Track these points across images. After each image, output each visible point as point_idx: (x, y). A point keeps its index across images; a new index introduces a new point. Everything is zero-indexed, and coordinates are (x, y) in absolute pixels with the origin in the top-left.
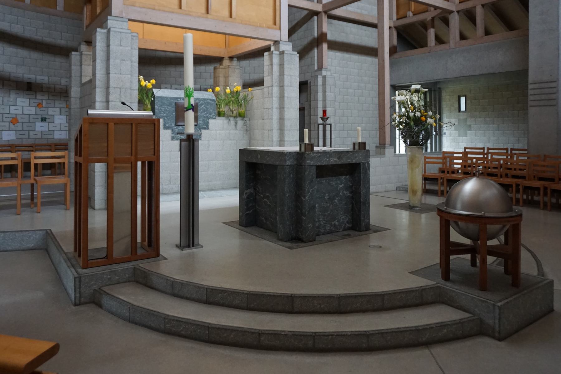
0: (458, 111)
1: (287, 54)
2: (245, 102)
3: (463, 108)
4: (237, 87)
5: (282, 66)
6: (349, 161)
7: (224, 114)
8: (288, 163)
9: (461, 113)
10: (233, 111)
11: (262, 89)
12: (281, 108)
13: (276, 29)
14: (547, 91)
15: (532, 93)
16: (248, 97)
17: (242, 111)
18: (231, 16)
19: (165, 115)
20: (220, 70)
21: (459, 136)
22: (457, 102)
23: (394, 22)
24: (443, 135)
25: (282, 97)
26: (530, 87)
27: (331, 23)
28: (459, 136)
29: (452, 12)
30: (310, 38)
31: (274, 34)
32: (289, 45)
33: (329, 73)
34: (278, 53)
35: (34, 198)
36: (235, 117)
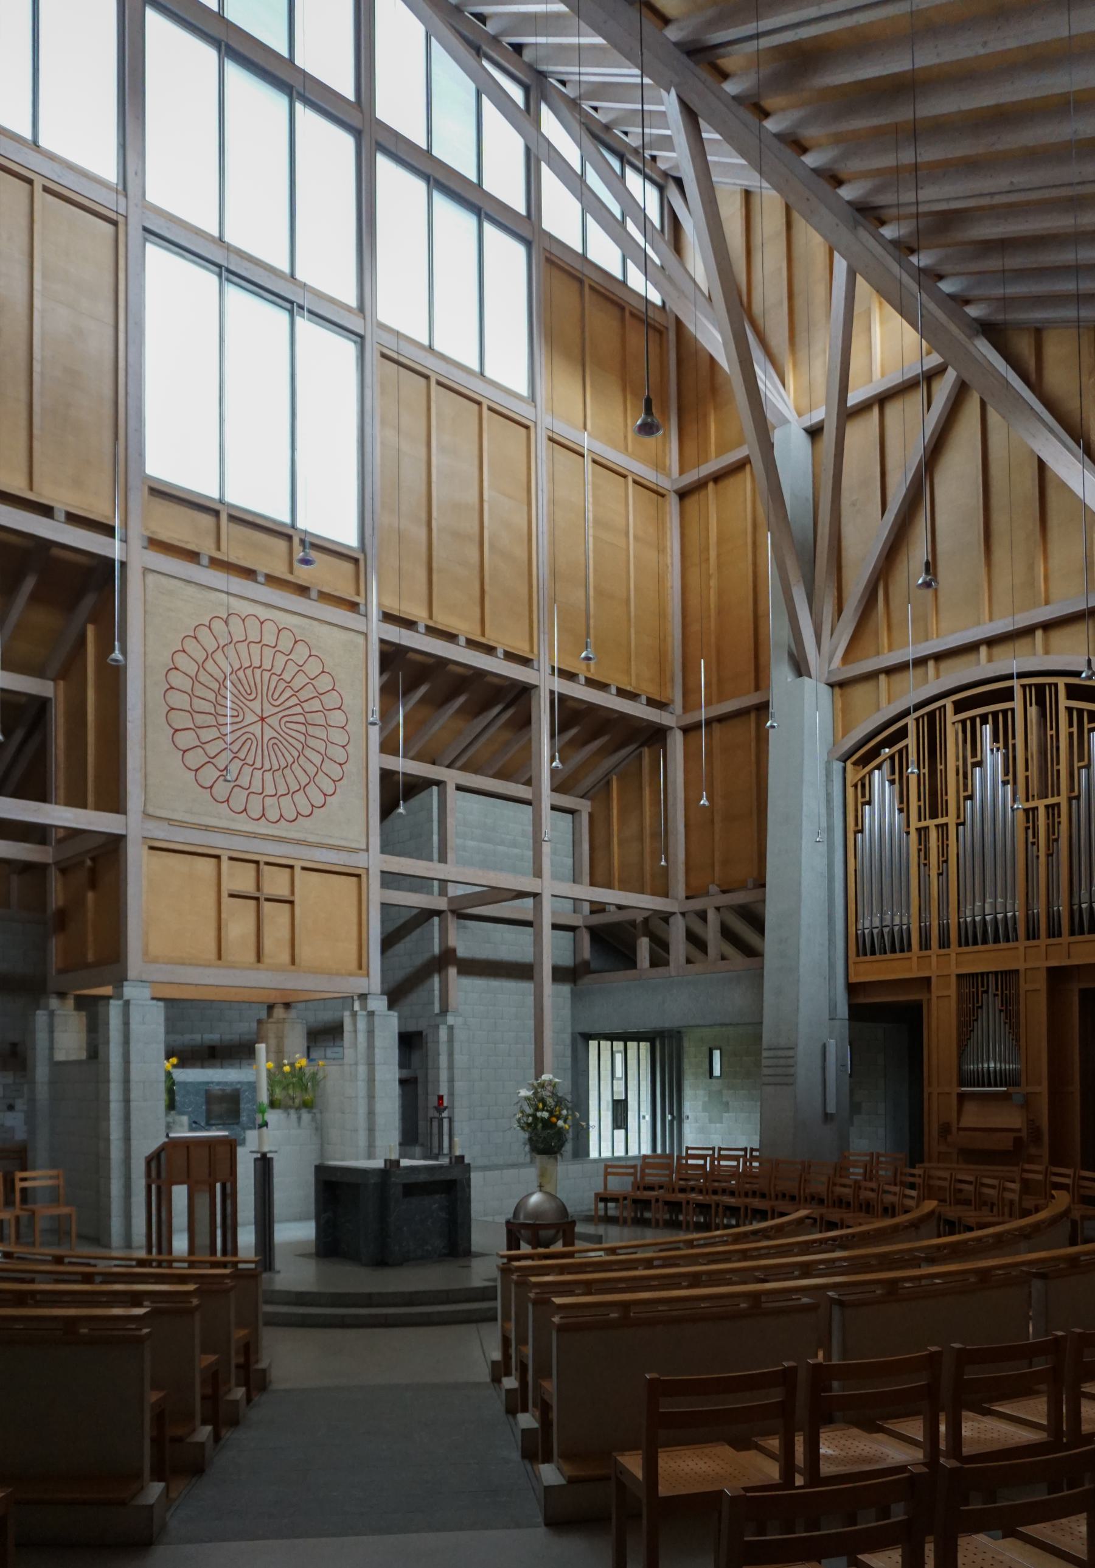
0: (708, 1075)
1: (379, 1015)
2: (313, 1086)
3: (717, 1072)
4: (300, 1060)
5: (371, 1032)
6: (442, 1177)
7: (280, 1104)
8: (373, 1181)
9: (713, 1081)
10: (293, 1099)
11: (340, 1065)
12: (371, 1097)
13: (362, 976)
14: (782, 1062)
15: (766, 1064)
16: (318, 1077)
17: (307, 1097)
18: (293, 962)
19: (190, 1109)
20: (269, 1025)
21: (711, 1121)
22: (707, 1060)
23: (585, 917)
24: (685, 1121)
25: (371, 1080)
26: (765, 1054)
27: (465, 927)
28: (711, 1121)
29: (674, 913)
30: (427, 956)
31: (359, 985)
32: (382, 1000)
33: (460, 1020)
34: (364, 1013)
35: (472, 1169)
36: (298, 1109)
